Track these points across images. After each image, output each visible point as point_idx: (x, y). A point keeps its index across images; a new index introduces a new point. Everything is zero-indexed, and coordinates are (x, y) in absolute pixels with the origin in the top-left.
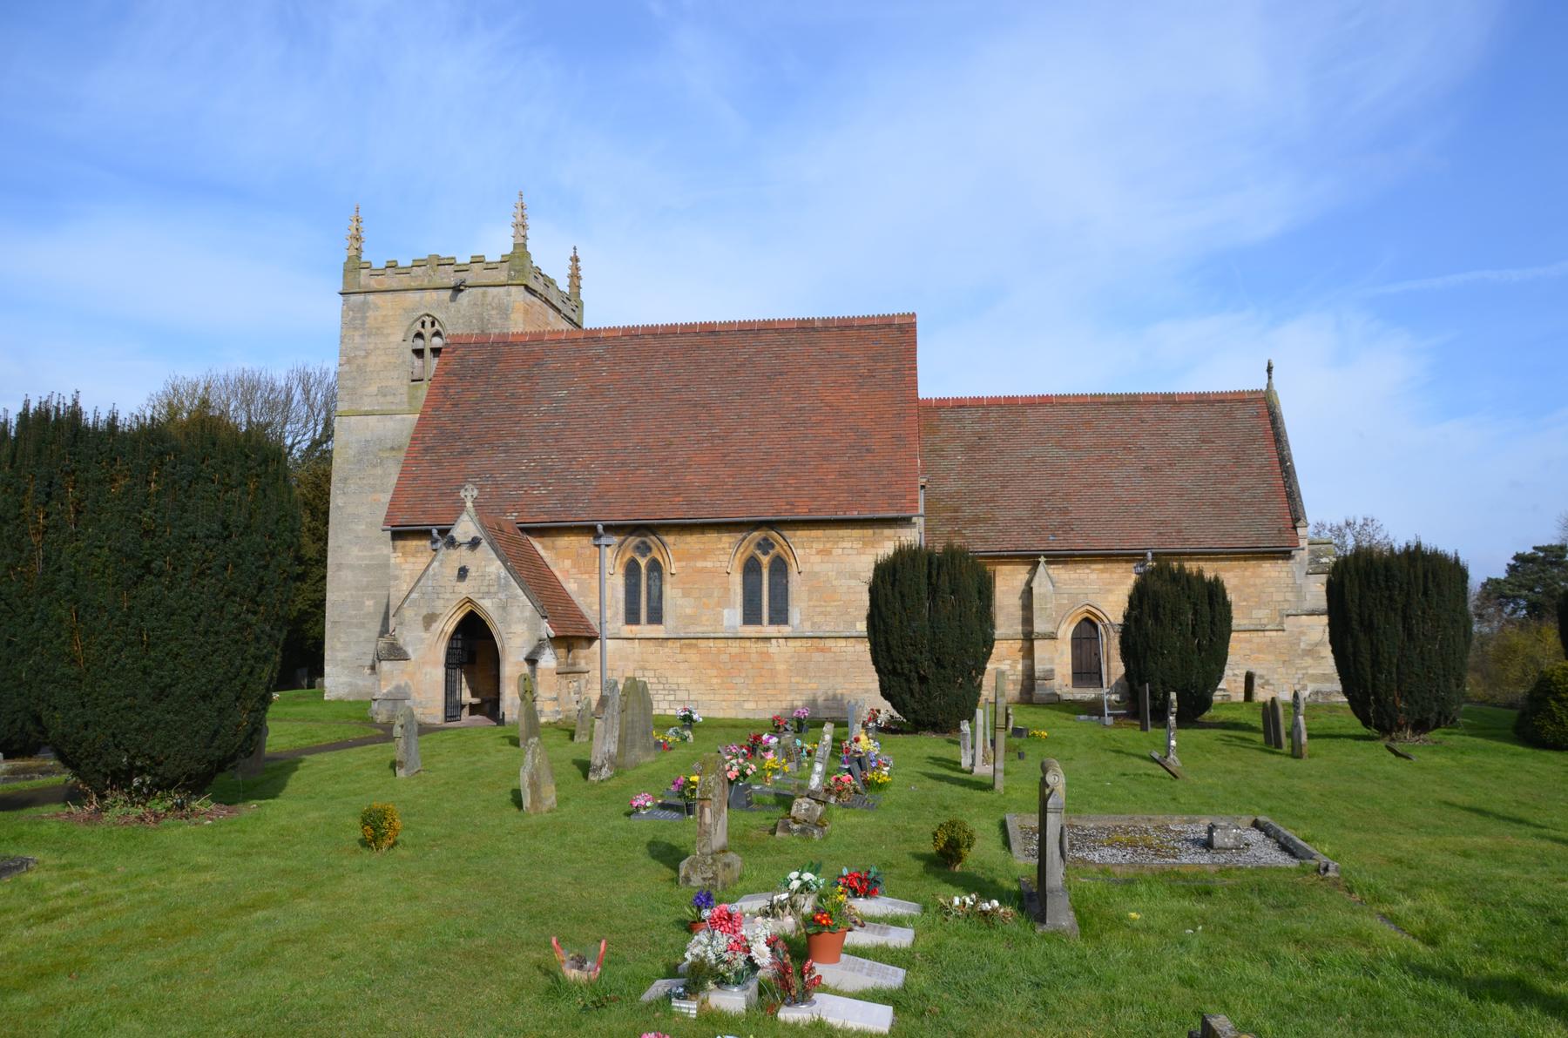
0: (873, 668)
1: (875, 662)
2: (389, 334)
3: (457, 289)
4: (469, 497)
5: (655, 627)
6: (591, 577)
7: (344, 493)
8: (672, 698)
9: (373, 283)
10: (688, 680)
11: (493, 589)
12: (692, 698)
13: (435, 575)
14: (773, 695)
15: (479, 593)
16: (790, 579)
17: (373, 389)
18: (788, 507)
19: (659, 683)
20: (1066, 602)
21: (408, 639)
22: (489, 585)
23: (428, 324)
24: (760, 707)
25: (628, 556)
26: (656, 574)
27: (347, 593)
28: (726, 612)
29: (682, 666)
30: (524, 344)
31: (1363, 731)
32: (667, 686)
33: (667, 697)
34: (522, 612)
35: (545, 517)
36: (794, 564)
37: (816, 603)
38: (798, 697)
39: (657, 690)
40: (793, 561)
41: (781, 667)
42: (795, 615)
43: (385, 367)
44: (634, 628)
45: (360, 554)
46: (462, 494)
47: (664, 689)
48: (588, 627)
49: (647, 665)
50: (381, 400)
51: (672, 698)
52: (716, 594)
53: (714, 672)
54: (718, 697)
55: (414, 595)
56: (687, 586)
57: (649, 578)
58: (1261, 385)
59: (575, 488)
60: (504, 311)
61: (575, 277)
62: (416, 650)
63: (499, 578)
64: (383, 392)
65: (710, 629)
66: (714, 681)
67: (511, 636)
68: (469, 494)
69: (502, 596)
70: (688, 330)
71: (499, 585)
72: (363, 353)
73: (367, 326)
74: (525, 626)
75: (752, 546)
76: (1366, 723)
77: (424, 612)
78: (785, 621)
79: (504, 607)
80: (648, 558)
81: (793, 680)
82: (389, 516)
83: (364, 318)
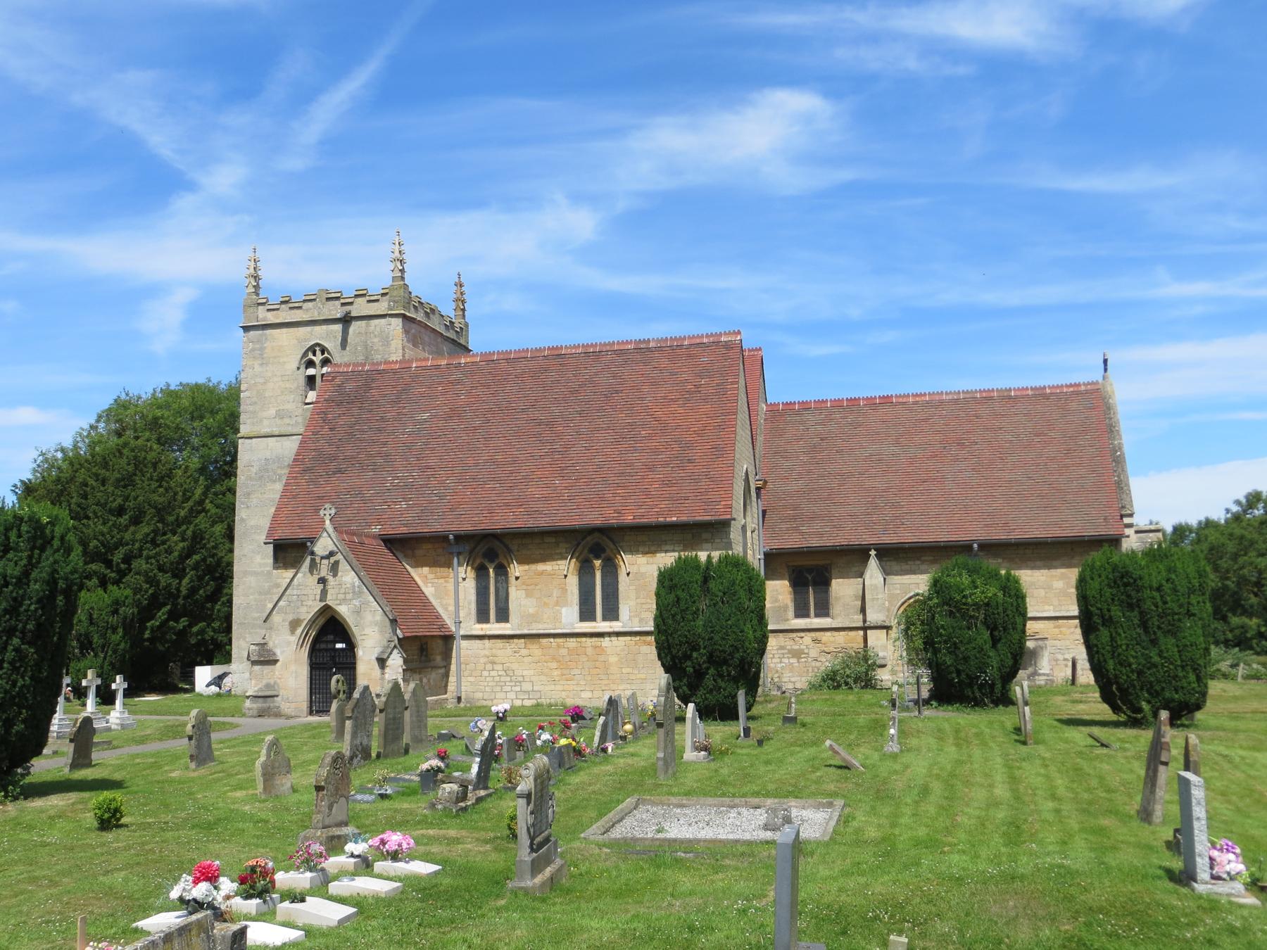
0: (660, 663)
1: (660, 657)
2: (285, 362)
3: (346, 320)
4: (328, 516)
5: (503, 625)
6: (446, 582)
7: (248, 507)
8: (518, 689)
9: (272, 318)
10: (532, 672)
11: (349, 596)
12: (535, 688)
13: (299, 585)
14: (606, 685)
15: (337, 599)
16: (620, 580)
17: (272, 412)
18: (616, 515)
19: (507, 675)
20: (899, 592)
21: (276, 642)
22: (345, 593)
23: (318, 353)
24: (595, 696)
25: (478, 562)
26: (503, 578)
27: (251, 597)
28: (564, 610)
29: (526, 659)
30: (395, 372)
31: (1114, 717)
32: (513, 678)
33: (513, 688)
34: (374, 616)
35: (404, 530)
36: (623, 566)
37: (643, 601)
38: (628, 687)
39: (505, 682)
40: (622, 563)
41: (613, 659)
42: (624, 611)
43: (282, 392)
44: (484, 626)
45: (263, 561)
46: (322, 513)
47: (511, 681)
48: (443, 626)
49: (496, 659)
50: (278, 421)
51: (518, 689)
52: (555, 595)
53: (554, 665)
54: (559, 687)
55: (281, 603)
56: (529, 587)
57: (496, 582)
58: (1097, 376)
59: (431, 502)
60: (386, 341)
61: (460, 301)
62: (284, 651)
63: (354, 586)
64: (280, 415)
65: (551, 626)
66: (556, 673)
67: (363, 637)
68: (328, 512)
69: (356, 602)
70: (537, 354)
71: (354, 592)
72: (261, 380)
73: (265, 355)
74: (376, 629)
75: (586, 551)
76: (1115, 709)
77: (290, 617)
78: (616, 618)
79: (358, 612)
80: (495, 564)
81: (624, 671)
82: (272, 529)
83: (262, 349)
